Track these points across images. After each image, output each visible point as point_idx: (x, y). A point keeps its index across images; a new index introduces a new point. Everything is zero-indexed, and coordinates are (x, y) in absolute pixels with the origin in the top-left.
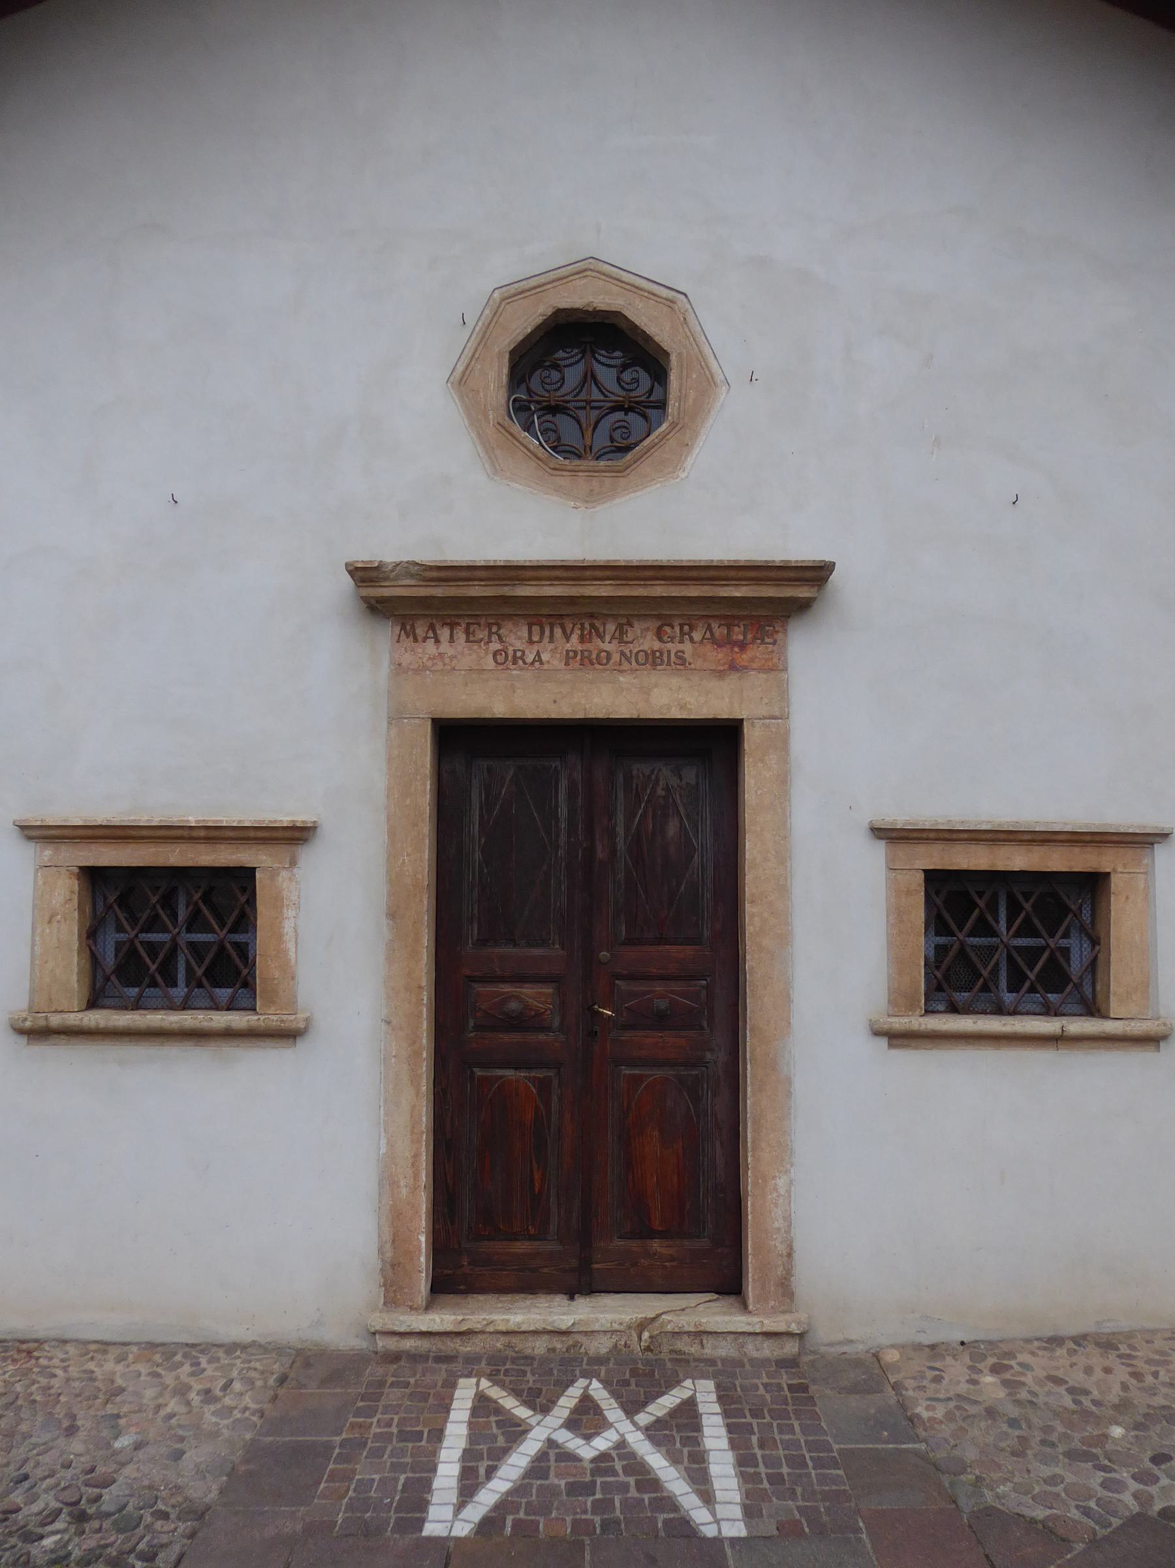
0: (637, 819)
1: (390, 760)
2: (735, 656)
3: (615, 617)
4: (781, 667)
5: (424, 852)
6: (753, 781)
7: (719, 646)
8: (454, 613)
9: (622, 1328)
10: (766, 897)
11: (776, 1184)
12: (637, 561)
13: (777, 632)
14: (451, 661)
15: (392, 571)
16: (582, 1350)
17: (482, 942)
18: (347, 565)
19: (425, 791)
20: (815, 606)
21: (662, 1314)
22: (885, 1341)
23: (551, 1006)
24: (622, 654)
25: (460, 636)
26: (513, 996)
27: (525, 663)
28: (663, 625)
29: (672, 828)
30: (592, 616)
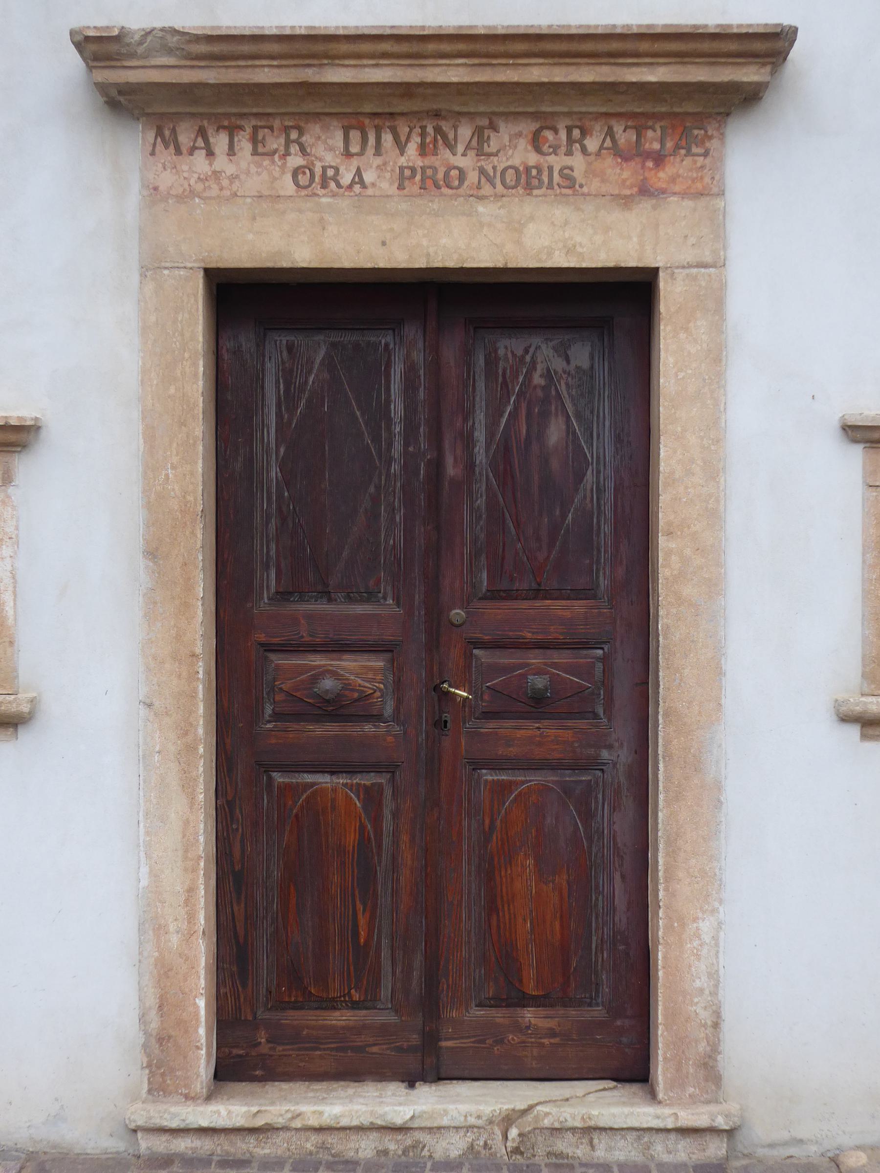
0: (504, 420)
1: (145, 330)
2: (646, 174)
3: (471, 116)
4: (715, 190)
5: (196, 463)
6: (671, 360)
7: (626, 159)
8: (234, 110)
9: (480, 1123)
10: (689, 527)
11: (698, 929)
12: (503, 27)
13: (710, 138)
14: (231, 183)
15: (140, 43)
16: (425, 1153)
17: (283, 596)
18: (72, 33)
19: (196, 375)
20: (769, 98)
21: (537, 1104)
22: (846, 1141)
23: (382, 686)
24: (482, 171)
25: (244, 145)
26: (328, 671)
27: (339, 186)
28: (542, 128)
29: (555, 433)
30: (437, 115)
